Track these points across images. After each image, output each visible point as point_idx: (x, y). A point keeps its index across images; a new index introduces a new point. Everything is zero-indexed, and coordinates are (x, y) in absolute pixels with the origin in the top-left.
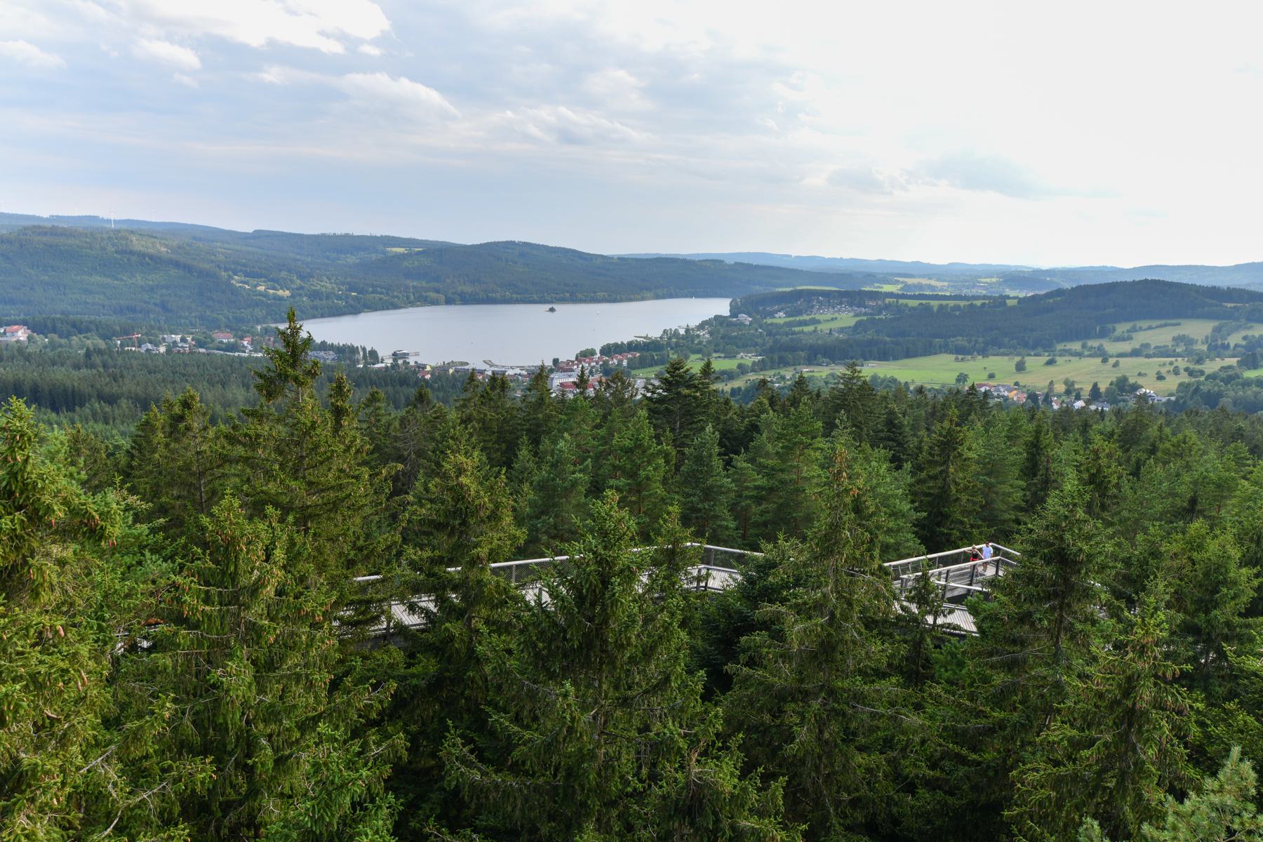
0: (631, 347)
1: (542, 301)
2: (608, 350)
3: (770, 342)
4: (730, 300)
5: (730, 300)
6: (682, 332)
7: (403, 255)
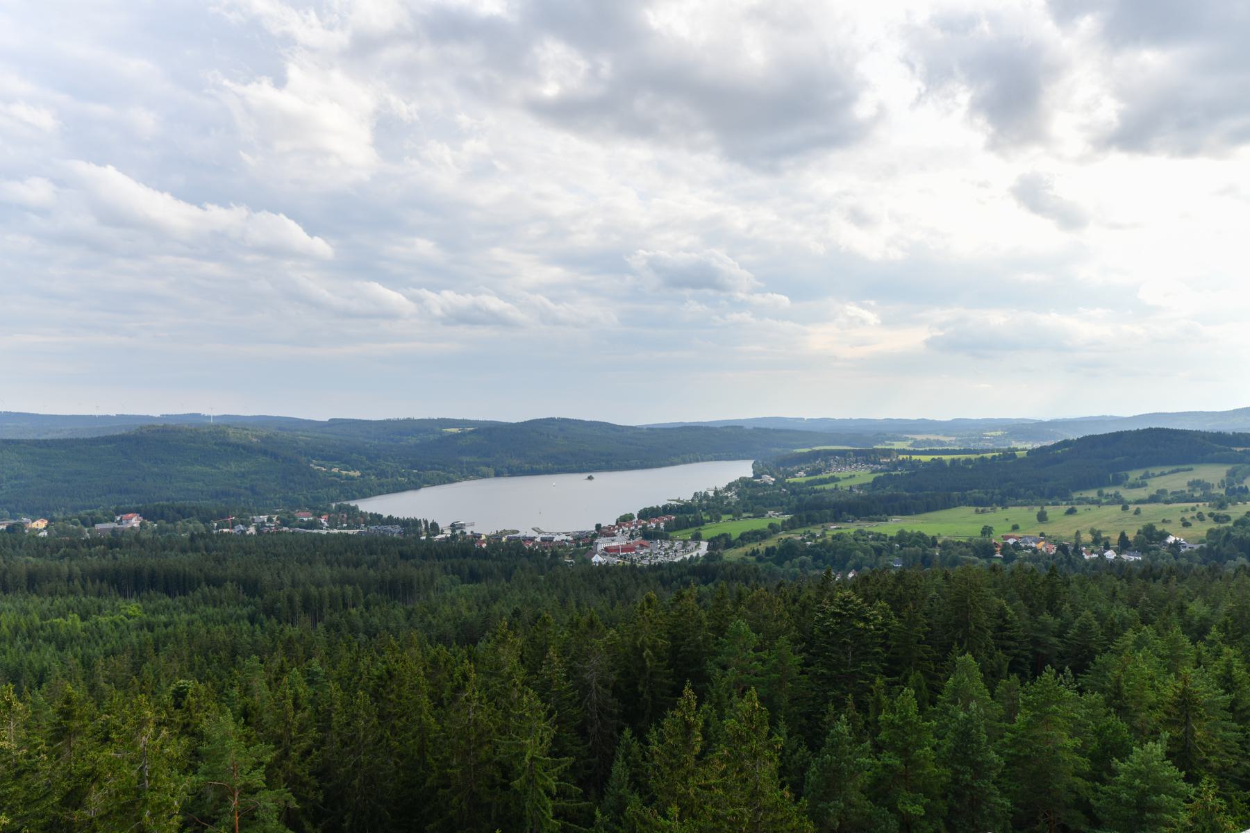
0: (666, 510)
1: (580, 470)
2: (646, 514)
3: (795, 503)
4: (752, 462)
5: (752, 462)
6: (711, 494)
7: (458, 434)
